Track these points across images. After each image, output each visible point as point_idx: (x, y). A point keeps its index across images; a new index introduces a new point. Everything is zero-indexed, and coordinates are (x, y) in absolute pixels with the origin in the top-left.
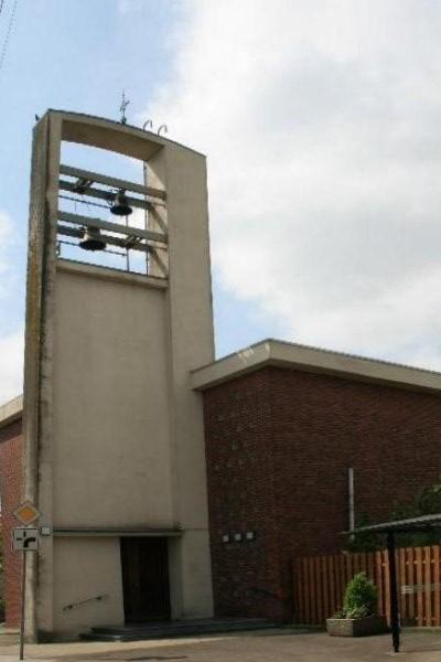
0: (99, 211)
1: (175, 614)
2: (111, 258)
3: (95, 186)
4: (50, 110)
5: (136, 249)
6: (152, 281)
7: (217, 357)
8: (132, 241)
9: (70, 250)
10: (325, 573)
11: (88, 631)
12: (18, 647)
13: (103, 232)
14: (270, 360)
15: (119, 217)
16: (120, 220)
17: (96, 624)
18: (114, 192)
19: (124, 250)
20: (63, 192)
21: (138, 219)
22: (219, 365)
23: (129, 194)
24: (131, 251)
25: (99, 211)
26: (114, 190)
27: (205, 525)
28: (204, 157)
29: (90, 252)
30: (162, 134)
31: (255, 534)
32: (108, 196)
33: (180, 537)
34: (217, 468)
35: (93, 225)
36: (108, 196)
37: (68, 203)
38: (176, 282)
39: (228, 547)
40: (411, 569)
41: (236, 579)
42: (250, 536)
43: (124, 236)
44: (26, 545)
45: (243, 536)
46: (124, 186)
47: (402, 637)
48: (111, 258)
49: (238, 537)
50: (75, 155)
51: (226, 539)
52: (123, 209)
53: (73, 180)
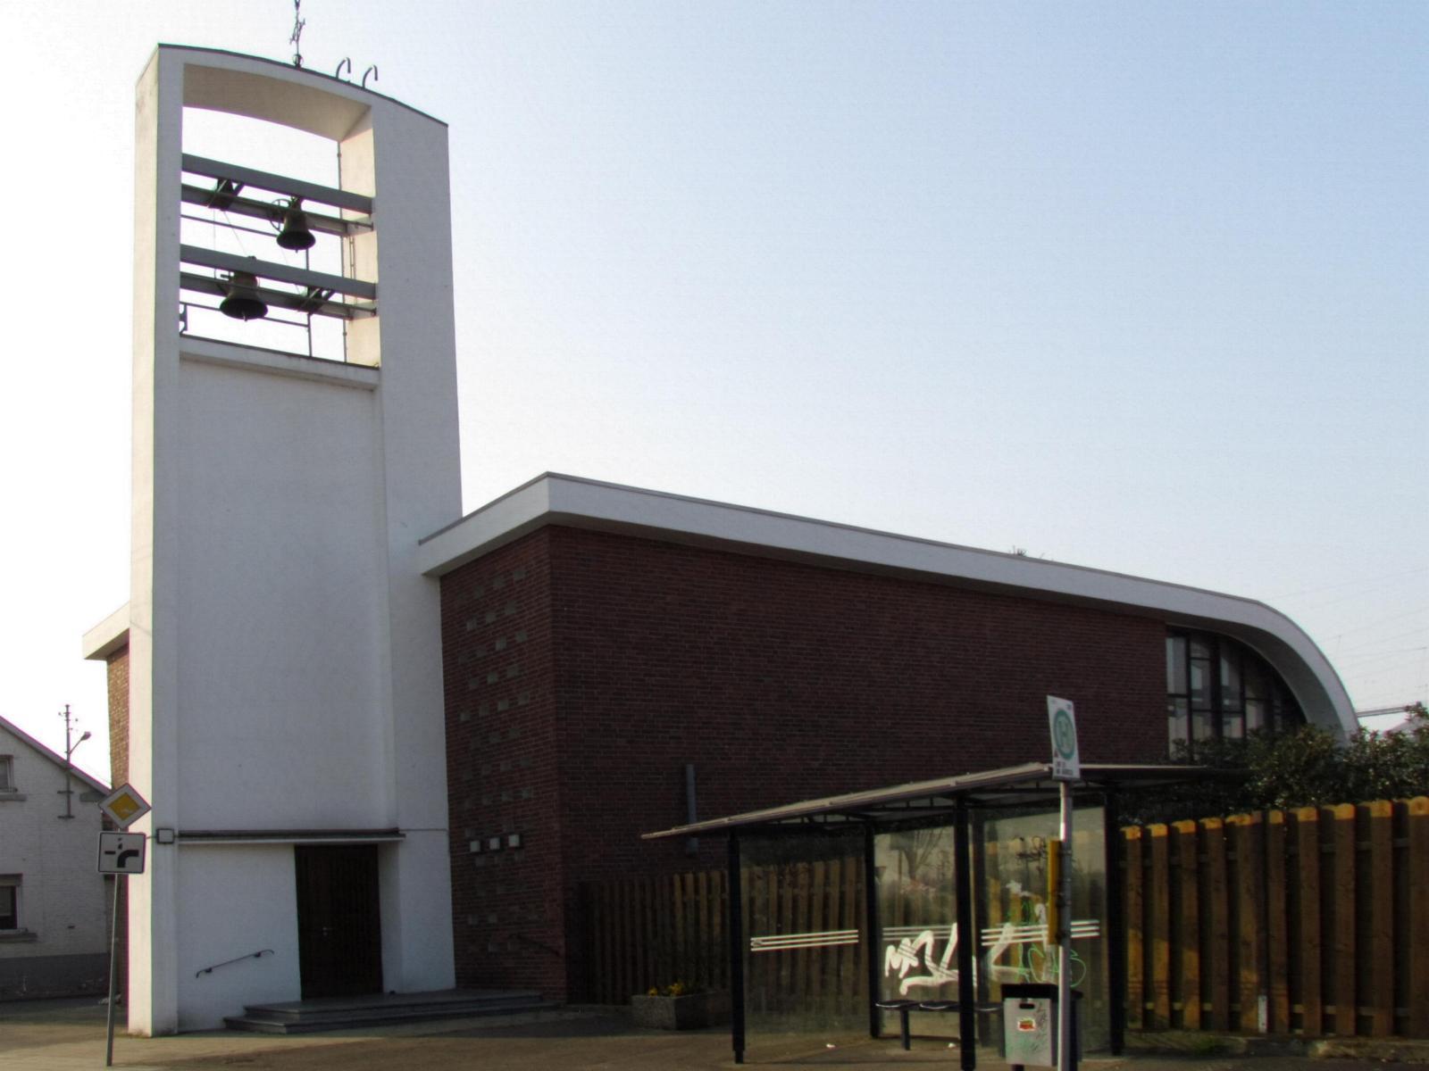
0: (255, 241)
1: (390, 984)
2: (277, 332)
3: (248, 193)
4: (161, 46)
5: (321, 313)
6: (351, 374)
7: (466, 512)
8: (315, 298)
9: (208, 320)
10: (704, 903)
11: (235, 1012)
12: (106, 1043)
13: (264, 283)
14: (550, 514)
15: (292, 252)
16: (293, 258)
17: (258, 1000)
18: (285, 204)
19: (301, 317)
20: (187, 208)
21: (325, 255)
22: (467, 523)
23: (308, 206)
24: (316, 318)
25: (255, 241)
26: (282, 200)
27: (443, 821)
28: (446, 125)
29: (240, 322)
30: (371, 84)
31: (521, 837)
32: (269, 212)
33: (396, 843)
34: (463, 717)
35: (245, 269)
36: (269, 212)
37: (207, 230)
38: (413, 393)
39: (480, 862)
40: (788, 904)
41: (493, 919)
42: (514, 841)
43: (300, 290)
44: (121, 863)
45: (504, 842)
46: (300, 190)
47: (752, 1040)
48: (277, 332)
49: (494, 844)
50: (217, 135)
51: (475, 846)
52: (297, 235)
53: (209, 184)
